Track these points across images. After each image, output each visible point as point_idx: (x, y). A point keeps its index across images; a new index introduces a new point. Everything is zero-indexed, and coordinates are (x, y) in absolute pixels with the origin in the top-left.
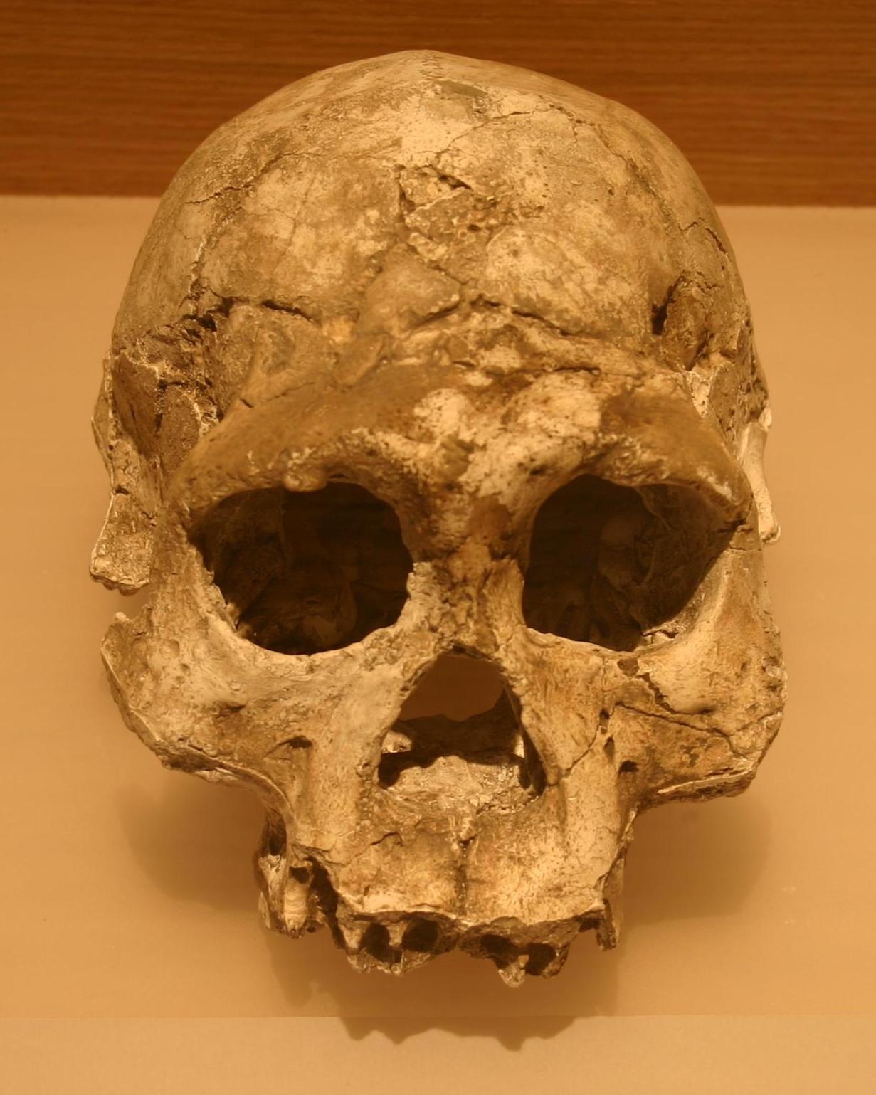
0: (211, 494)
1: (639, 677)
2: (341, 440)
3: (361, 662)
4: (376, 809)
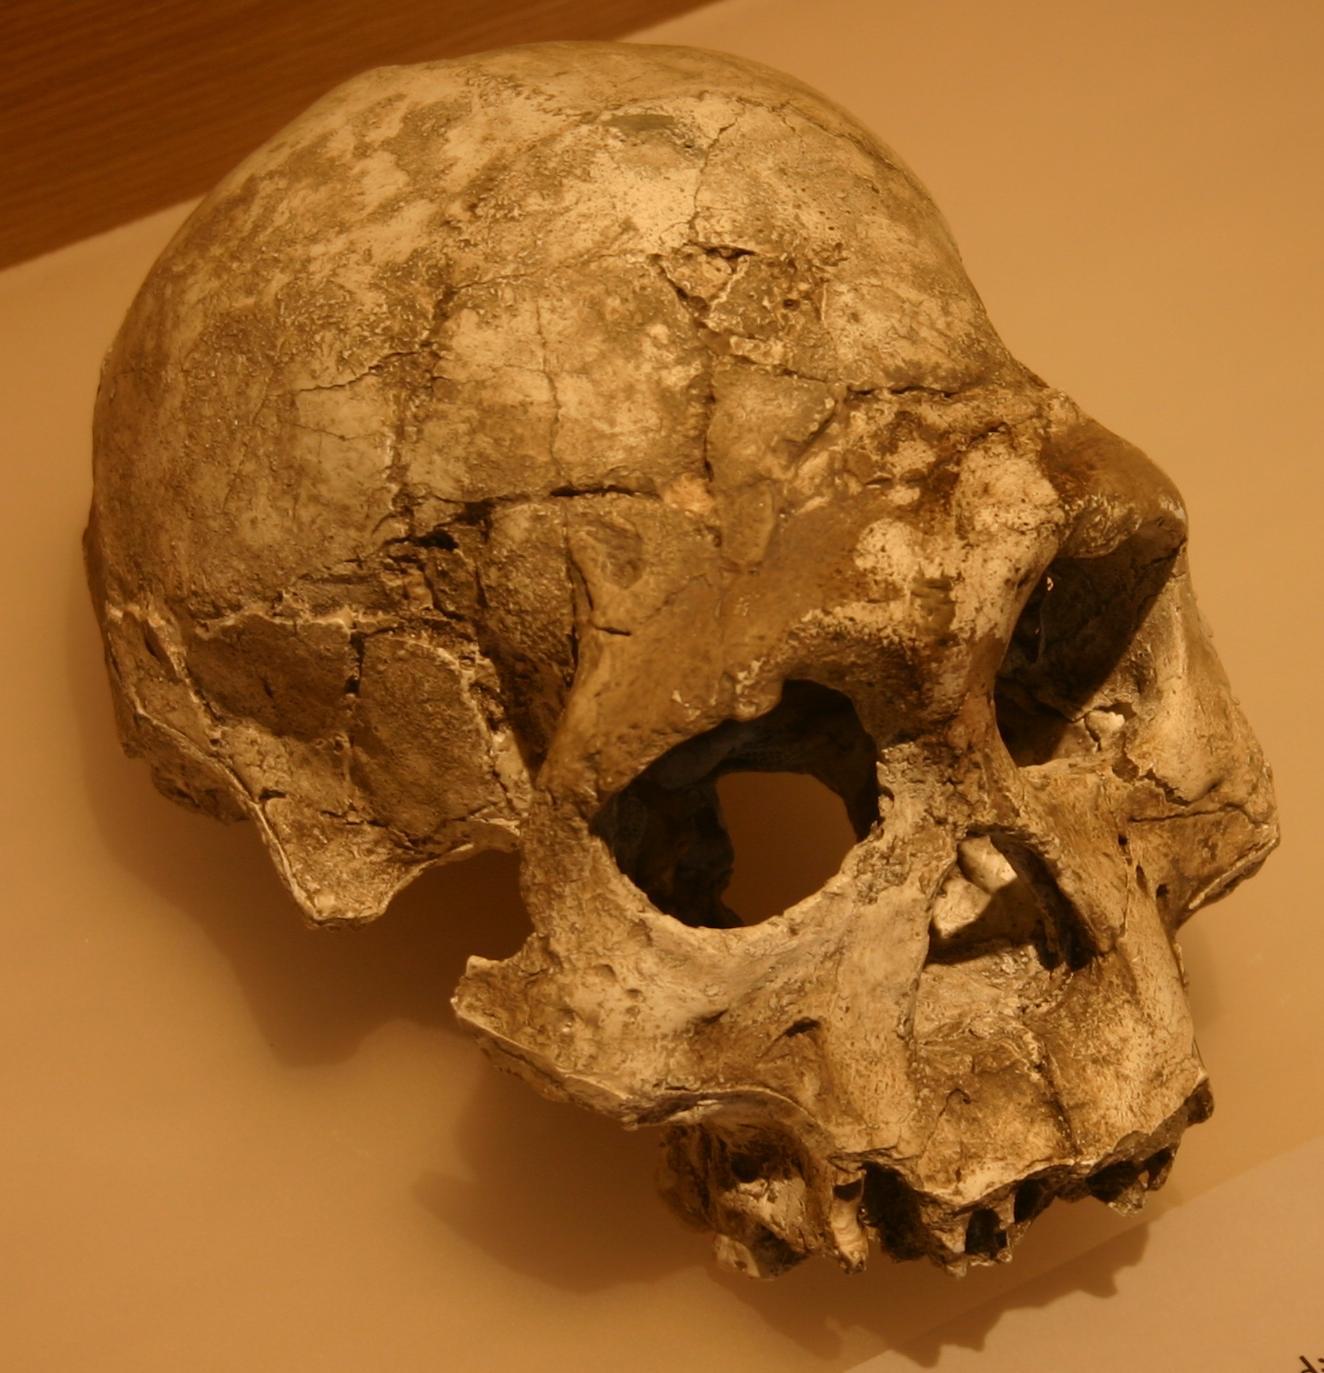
0: (633, 763)
1: (1141, 779)
2: (793, 635)
3: (854, 896)
4: (928, 1069)
